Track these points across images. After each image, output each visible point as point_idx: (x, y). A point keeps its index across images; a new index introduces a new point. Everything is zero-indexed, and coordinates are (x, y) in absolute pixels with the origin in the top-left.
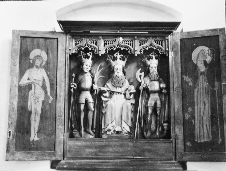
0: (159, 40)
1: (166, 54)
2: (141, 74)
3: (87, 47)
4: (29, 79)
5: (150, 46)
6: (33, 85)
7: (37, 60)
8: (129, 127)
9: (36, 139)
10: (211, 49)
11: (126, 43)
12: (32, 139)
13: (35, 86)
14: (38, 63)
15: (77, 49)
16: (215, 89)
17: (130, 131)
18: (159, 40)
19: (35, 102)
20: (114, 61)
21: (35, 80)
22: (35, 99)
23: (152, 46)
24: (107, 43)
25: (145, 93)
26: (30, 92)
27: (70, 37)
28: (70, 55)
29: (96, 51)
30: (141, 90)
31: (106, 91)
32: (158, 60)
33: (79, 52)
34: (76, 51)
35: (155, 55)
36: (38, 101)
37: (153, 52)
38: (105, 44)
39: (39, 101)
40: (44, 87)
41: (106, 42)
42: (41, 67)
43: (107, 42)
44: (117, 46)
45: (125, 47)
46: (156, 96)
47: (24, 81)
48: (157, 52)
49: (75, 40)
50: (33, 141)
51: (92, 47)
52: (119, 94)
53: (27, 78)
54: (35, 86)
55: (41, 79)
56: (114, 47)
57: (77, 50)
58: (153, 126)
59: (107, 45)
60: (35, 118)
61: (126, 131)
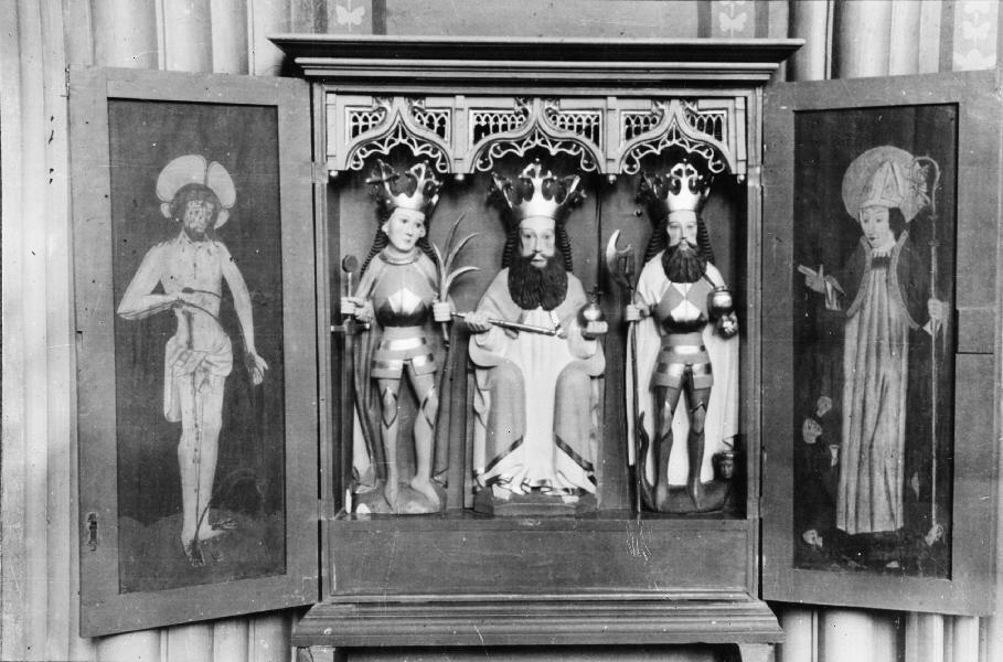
4: (159, 289)
6: (178, 313)
7: (193, 206)
9: (207, 531)
10: (922, 163)
11: (571, 128)
12: (187, 536)
13: (190, 318)
14: (196, 215)
16: (927, 328)
19: (193, 384)
21: (188, 291)
22: (193, 374)
24: (487, 126)
26: (171, 346)
28: (330, 177)
36: (206, 381)
37: (699, 174)
39: (211, 377)
40: (228, 320)
42: (211, 232)
47: (139, 300)
50: (194, 543)
51: (423, 143)
53: (152, 286)
54: (190, 318)
55: (214, 287)
57: (361, 157)
59: (487, 133)
60: (196, 450)
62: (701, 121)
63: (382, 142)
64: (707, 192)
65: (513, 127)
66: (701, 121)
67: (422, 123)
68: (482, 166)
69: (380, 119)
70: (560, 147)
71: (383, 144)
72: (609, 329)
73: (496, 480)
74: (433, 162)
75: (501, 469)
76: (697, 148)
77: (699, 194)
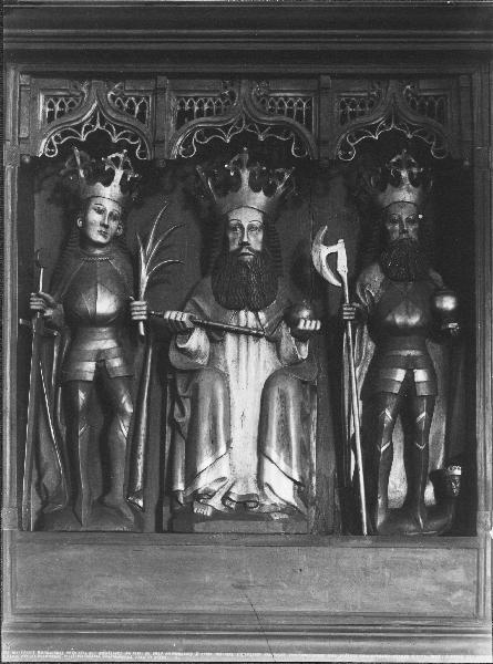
0: (288, 94)
1: (462, 160)
2: (332, 249)
3: (104, 128)
5: (388, 122)
8: (292, 483)
11: (281, 112)
15: (57, 139)
17: (293, 502)
18: (288, 94)
20: (225, 194)
23: (396, 123)
24: (192, 110)
25: (365, 335)
27: (23, 79)
28: (22, 163)
29: (143, 147)
30: (139, 321)
31: (189, 325)
32: (424, 188)
33: (66, 151)
34: (51, 146)
35: (125, 167)
37: (121, 152)
38: (183, 117)
41: (187, 108)
43: (191, 104)
44: (240, 125)
45: (278, 128)
46: (105, 342)
48: (419, 151)
49: (178, 98)
51: (123, 129)
52: (251, 338)
56: (226, 128)
57: (55, 143)
58: (398, 482)
59: (191, 118)
61: (277, 501)
62: (422, 105)
63: (119, 129)
64: (134, 195)
65: (218, 111)
66: (422, 105)
67: (121, 107)
68: (184, 153)
69: (77, 104)
70: (270, 132)
71: (227, 132)
72: (452, 295)
73: (197, 497)
74: (132, 149)
75: (203, 483)
76: (419, 133)
77: (128, 193)
